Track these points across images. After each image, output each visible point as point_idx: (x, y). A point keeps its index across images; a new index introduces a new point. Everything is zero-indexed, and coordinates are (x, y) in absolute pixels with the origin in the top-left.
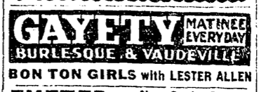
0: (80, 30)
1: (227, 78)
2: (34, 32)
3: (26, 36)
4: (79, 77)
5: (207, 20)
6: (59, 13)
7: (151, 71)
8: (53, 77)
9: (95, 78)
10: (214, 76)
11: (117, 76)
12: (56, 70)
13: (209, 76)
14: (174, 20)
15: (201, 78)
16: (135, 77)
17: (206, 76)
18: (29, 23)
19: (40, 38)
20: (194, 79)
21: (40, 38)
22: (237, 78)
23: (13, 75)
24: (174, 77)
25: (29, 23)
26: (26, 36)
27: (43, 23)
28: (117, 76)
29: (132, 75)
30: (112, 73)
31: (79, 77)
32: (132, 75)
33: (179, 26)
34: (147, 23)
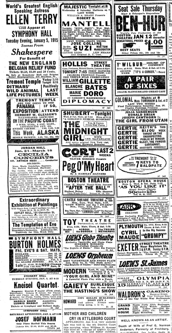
1: (13, 22)
4: (39, 237)
5: (95, 86)
7: (51, 282)
8: (117, 122)
9: (94, 134)
10: (127, 92)
11: (135, 121)
12: (67, 220)
13: (81, 188)
15: (9, 22)
16: (99, 291)
17: (80, 188)
20: (16, 36)
22: (15, 23)
23: (87, 88)
24: (13, 22)
28: (135, 121)
29: (105, 88)
30: (96, 93)
31: (39, 237)
32: (105, 88)
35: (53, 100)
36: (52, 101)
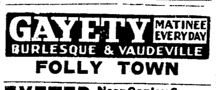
0: (66, 30)
2: (26, 31)
3: (20, 34)
6: (49, 15)
14: (145, 22)
18: (22, 24)
19: (32, 35)
21: (32, 35)
25: (22, 24)
26: (20, 34)
27: (34, 24)
33: (149, 27)
34: (123, 25)
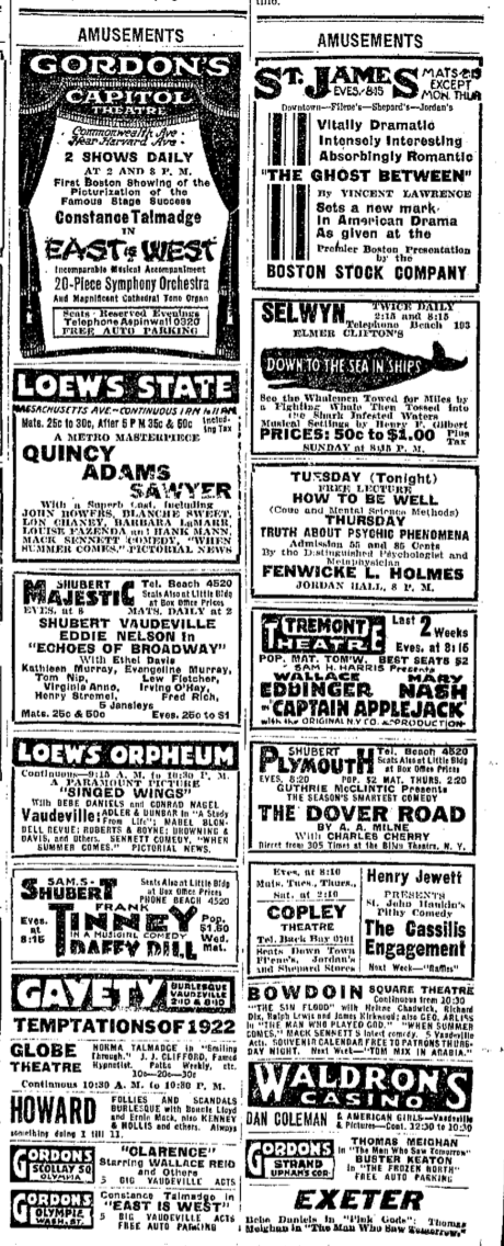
35: (318, 911)
36: (312, 916)
